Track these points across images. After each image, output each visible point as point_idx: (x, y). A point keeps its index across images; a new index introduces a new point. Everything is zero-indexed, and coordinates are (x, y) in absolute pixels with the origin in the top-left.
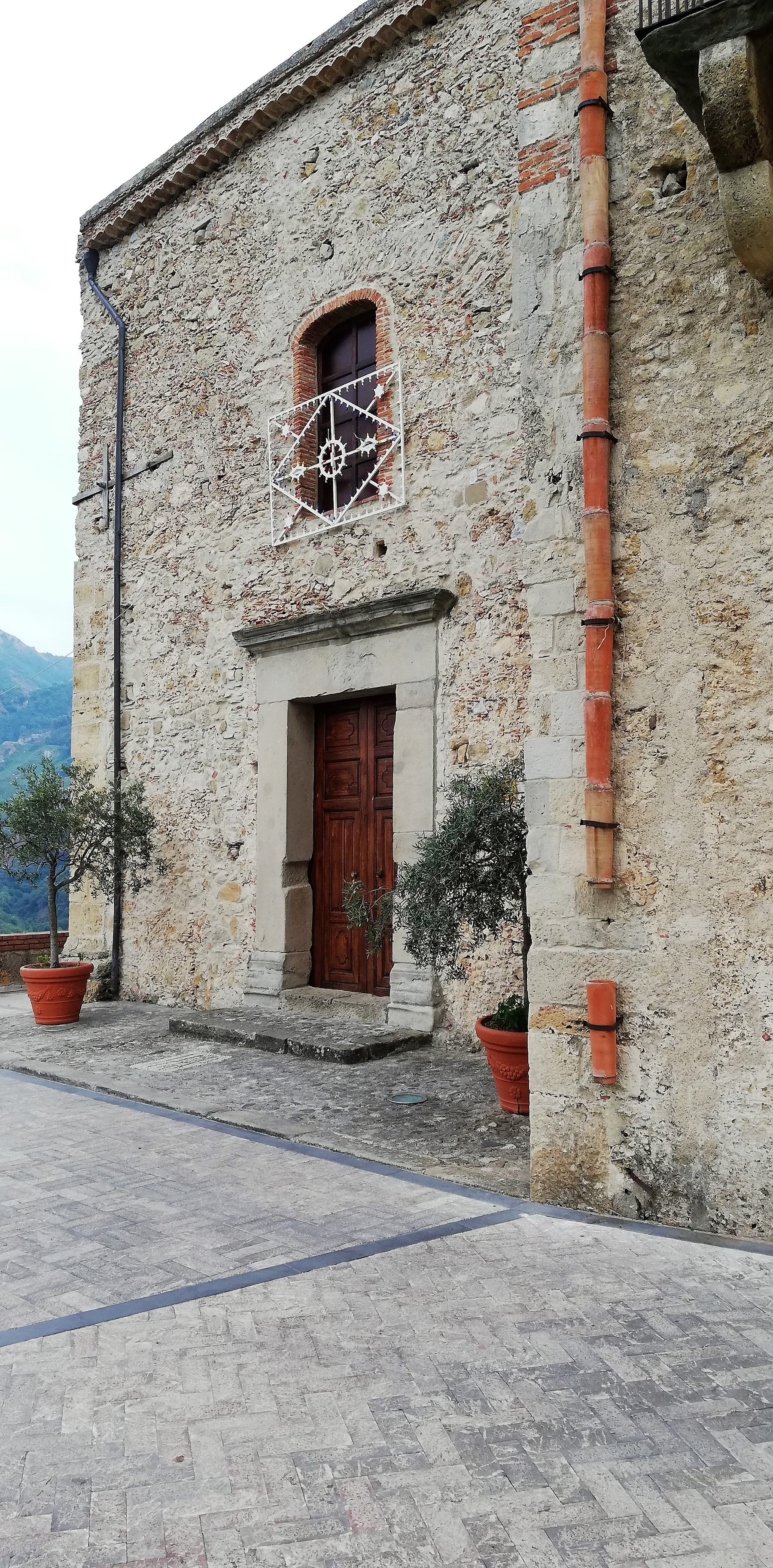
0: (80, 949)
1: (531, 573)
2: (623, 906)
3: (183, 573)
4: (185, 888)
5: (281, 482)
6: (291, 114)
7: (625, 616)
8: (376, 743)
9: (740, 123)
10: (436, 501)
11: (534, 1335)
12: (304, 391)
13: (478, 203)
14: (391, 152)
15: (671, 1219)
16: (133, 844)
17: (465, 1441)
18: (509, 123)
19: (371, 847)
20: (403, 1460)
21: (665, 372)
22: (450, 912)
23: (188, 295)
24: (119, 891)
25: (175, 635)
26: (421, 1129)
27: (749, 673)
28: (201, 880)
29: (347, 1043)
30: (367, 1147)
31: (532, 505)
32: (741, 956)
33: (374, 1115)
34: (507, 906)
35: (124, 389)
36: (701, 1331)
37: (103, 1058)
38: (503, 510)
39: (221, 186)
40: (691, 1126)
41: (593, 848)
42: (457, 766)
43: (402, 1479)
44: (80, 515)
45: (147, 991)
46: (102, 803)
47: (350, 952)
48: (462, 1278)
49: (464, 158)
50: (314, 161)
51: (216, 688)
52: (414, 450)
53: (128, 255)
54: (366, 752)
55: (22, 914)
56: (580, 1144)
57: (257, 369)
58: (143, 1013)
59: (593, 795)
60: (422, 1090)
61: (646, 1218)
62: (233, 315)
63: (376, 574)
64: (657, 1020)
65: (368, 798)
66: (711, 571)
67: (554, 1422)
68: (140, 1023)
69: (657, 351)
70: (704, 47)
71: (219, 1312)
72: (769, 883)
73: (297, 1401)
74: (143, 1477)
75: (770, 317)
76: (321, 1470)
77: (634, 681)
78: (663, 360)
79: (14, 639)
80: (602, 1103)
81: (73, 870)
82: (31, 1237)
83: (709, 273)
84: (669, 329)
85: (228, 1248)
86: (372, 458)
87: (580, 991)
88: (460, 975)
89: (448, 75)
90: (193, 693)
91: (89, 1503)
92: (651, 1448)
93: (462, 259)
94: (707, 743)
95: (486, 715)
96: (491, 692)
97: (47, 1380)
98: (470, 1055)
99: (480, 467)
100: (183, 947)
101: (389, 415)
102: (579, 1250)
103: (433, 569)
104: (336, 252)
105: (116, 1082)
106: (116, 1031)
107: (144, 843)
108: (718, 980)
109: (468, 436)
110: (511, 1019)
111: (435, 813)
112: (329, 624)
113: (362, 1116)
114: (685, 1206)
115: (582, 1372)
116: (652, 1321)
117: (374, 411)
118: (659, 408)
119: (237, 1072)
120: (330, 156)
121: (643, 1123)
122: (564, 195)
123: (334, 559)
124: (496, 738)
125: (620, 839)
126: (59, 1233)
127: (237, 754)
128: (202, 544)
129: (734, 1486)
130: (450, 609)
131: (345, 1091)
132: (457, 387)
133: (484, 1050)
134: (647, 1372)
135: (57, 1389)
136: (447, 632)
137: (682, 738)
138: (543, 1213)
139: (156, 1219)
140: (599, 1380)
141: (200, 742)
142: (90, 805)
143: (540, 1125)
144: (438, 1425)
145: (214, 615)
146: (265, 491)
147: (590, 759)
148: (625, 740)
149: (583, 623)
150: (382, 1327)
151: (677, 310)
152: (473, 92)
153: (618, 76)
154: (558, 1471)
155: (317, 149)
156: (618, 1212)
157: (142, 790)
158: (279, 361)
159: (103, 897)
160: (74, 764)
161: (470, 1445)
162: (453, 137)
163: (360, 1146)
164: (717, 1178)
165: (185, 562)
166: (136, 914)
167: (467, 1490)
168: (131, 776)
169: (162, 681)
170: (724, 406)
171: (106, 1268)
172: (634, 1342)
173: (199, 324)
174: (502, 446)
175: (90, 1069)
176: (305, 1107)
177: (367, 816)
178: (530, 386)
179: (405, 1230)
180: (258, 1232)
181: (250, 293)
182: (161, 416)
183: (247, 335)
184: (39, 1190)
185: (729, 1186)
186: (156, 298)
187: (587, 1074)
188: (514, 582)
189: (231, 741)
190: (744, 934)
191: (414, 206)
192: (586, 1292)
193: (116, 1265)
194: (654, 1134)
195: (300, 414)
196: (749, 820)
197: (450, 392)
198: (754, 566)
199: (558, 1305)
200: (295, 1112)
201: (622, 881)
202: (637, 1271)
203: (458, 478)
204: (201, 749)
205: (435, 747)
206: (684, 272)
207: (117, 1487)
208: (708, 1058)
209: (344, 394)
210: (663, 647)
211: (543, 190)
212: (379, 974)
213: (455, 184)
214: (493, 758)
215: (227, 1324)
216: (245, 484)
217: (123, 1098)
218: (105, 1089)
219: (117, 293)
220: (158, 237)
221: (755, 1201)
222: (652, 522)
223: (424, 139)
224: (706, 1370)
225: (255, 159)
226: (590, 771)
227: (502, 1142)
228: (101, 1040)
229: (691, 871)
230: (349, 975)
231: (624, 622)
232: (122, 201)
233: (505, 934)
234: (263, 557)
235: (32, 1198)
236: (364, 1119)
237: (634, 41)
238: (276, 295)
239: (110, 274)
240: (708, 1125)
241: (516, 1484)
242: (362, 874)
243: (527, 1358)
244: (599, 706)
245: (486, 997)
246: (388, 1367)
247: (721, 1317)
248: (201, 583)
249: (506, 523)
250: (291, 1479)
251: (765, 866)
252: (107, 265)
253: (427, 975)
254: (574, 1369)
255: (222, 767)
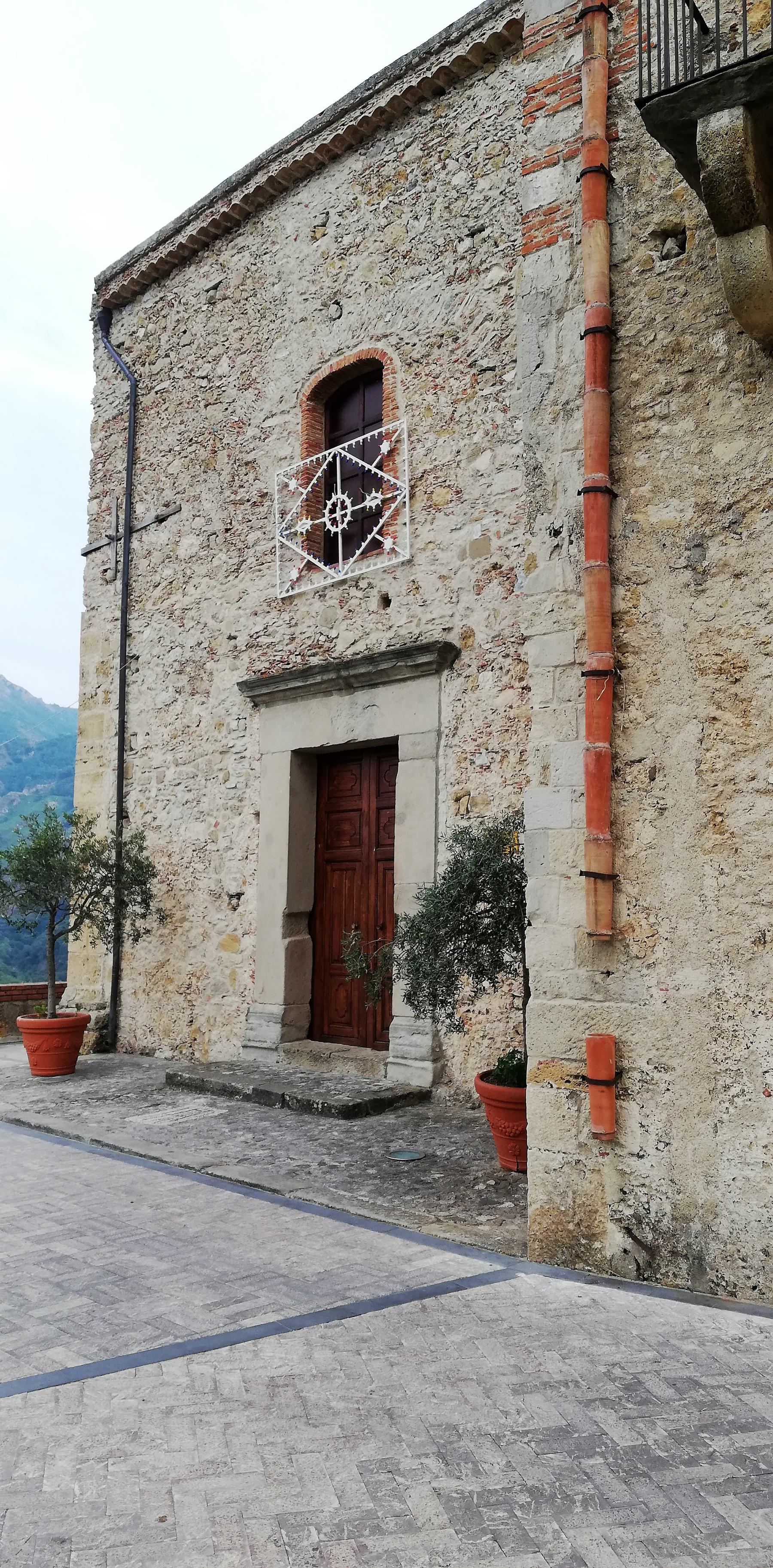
0: (78, 1000)
1: (531, 624)
2: (623, 959)
3: (189, 624)
4: (184, 938)
5: (287, 536)
6: (302, 180)
7: (625, 668)
8: (379, 794)
9: (737, 189)
10: (441, 555)
11: (528, 1397)
12: (312, 447)
13: (484, 266)
14: (399, 217)
15: (670, 1280)
16: (133, 893)
17: (456, 1505)
18: (515, 189)
19: (373, 897)
20: (390, 1524)
21: (665, 429)
22: (450, 964)
23: (199, 352)
24: (118, 942)
25: (180, 685)
26: (418, 1186)
27: (749, 725)
28: (201, 930)
29: (344, 1098)
30: (362, 1204)
31: (533, 558)
32: (740, 1010)
33: (371, 1171)
34: (507, 958)
35: (134, 443)
36: (699, 1395)
37: (97, 1110)
38: (506, 565)
39: (233, 248)
40: (691, 1184)
41: (592, 899)
42: (459, 817)
43: (390, 1542)
44: (88, 566)
45: (144, 1043)
46: (103, 852)
47: (350, 1005)
48: (456, 1338)
49: (471, 223)
50: (324, 225)
51: (220, 738)
52: (419, 503)
53: (142, 314)
54: (368, 803)
55: (23, 967)
56: (578, 1201)
57: (266, 425)
58: (139, 1066)
59: (592, 847)
60: (421, 1147)
61: (645, 1279)
62: (242, 373)
63: (380, 626)
64: (657, 1075)
65: (370, 848)
66: (711, 624)
67: (546, 1486)
68: (136, 1075)
69: (657, 408)
70: (702, 116)
71: (208, 1370)
72: (769, 936)
73: (284, 1462)
74: (124, 1537)
75: (769, 376)
76: (306, 1532)
77: (634, 732)
78: (663, 418)
79: (21, 690)
80: (600, 1159)
81: (72, 920)
82: (19, 1291)
83: (708, 334)
84: (669, 387)
85: (217, 1304)
86: (378, 512)
87: (580, 1044)
88: (459, 1028)
89: (455, 144)
90: (197, 743)
91: (69, 1563)
92: (645, 1514)
93: (468, 320)
94: (706, 795)
95: (489, 767)
96: (494, 744)
97: (30, 1437)
98: (470, 1112)
99: (484, 522)
100: (182, 997)
101: (395, 471)
102: (576, 1311)
103: (436, 622)
104: (345, 312)
105: (110, 1135)
106: (112, 1083)
107: (144, 892)
108: (718, 1034)
109: (472, 492)
110: (510, 1074)
111: (436, 864)
112: (333, 676)
113: (358, 1172)
114: (684, 1266)
115: (576, 1435)
116: (649, 1385)
117: (380, 467)
118: (659, 464)
119: (233, 1126)
120: (340, 220)
121: (642, 1181)
122: (566, 258)
123: (339, 611)
124: (498, 790)
125: (619, 891)
126: (47, 1287)
127: (239, 804)
128: (208, 595)
129: (729, 1554)
130: (453, 662)
131: (341, 1146)
132: (462, 444)
133: (483, 1106)
134: (642, 1436)
135: (40, 1446)
136: (450, 685)
137: (681, 789)
138: (540, 1273)
139: (147, 1274)
140: (594, 1443)
141: (203, 792)
142: (91, 855)
143: (538, 1181)
144: (427, 1489)
145: (220, 666)
146: (271, 544)
147: (589, 810)
148: (624, 791)
149: (583, 674)
150: (373, 1387)
151: (676, 369)
152: (480, 160)
153: (619, 144)
154: (549, 1536)
155: (328, 213)
156: (616, 1272)
157: (143, 838)
158: (287, 417)
159: (102, 947)
160: (77, 812)
161: (460, 1509)
162: (460, 203)
163: (355, 1202)
164: (717, 1237)
165: (191, 613)
166: (135, 964)
167: (456, 1555)
168: (133, 826)
169: (166, 731)
170: (723, 462)
171: (94, 1323)
172: (629, 1406)
173: (209, 380)
174: (506, 501)
175: (84, 1121)
176: (300, 1163)
177: (368, 867)
178: (532, 442)
179: (399, 1288)
180: (249, 1289)
181: (260, 351)
182: (170, 470)
183: (256, 392)
184: (29, 1243)
185: (729, 1246)
186: (167, 356)
187: (586, 1130)
188: (517, 635)
189: (234, 791)
190: (744, 987)
191: (421, 269)
192: (582, 1353)
193: (104, 1320)
194: (654, 1192)
195: (307, 469)
196: (749, 872)
197: (455, 448)
198: (754, 620)
199: (553, 1366)
200: (291, 1168)
201: (622, 933)
202: (635, 1333)
203: (462, 532)
204: (203, 799)
205: (436, 798)
206: (683, 332)
207: (97, 1547)
208: (708, 1115)
209: (350, 450)
210: (663, 699)
211: (545, 253)
212: (379, 1026)
213: (462, 247)
214: (495, 810)
215: (215, 1381)
216: (252, 538)
217: (116, 1151)
218: (98, 1142)
219: (129, 350)
220: (170, 296)
221: (756, 1263)
222: (652, 576)
223: (432, 204)
224: (703, 1435)
225: (267, 223)
226: (589, 822)
227: (501, 1200)
228: (96, 1092)
229: (691, 924)
230: (348, 1029)
231: (623, 674)
232: (136, 262)
233: (506, 988)
234: (268, 609)
235: (21, 1252)
236: (360, 1176)
237: (635, 111)
238: (285, 353)
239: (123, 332)
240: (708, 1183)
241: (505, 1550)
242: (363, 926)
243: (521, 1420)
244: (599, 757)
245: (486, 1052)
246: (378, 1428)
247: (721, 1380)
248: (207, 634)
249: (509, 578)
250: (276, 1542)
251: (765, 919)
252: (120, 324)
253: (427, 1030)
254: (568, 1432)
255: (224, 816)
